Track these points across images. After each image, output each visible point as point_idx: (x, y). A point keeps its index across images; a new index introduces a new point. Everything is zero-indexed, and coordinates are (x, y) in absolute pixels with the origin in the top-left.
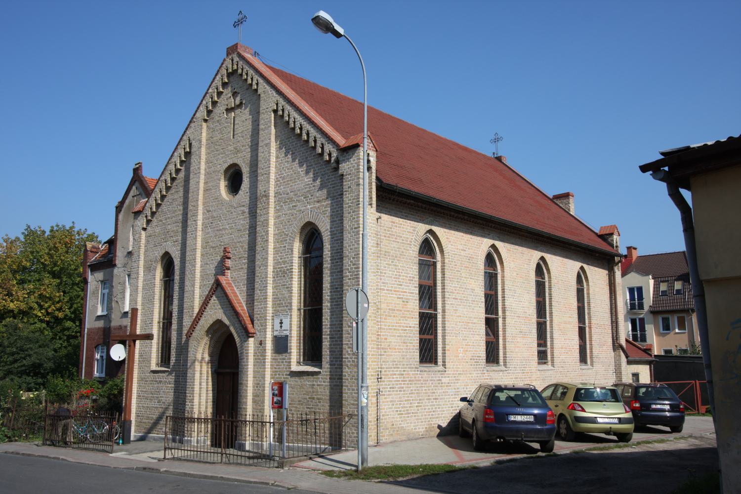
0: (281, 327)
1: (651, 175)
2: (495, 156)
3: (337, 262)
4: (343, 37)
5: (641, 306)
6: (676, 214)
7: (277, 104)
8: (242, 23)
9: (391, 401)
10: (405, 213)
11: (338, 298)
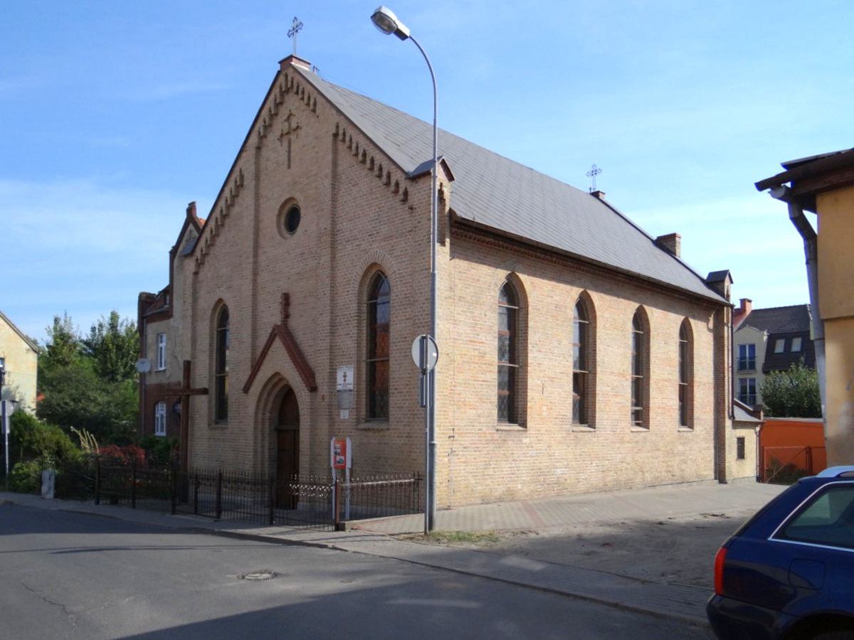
0: (345, 380)
1: (769, 192)
2: (592, 191)
3: (406, 308)
4: (409, 39)
5: (752, 366)
6: (798, 241)
7: (337, 127)
8: (297, 31)
9: (464, 462)
10: (484, 253)
11: (407, 349)
